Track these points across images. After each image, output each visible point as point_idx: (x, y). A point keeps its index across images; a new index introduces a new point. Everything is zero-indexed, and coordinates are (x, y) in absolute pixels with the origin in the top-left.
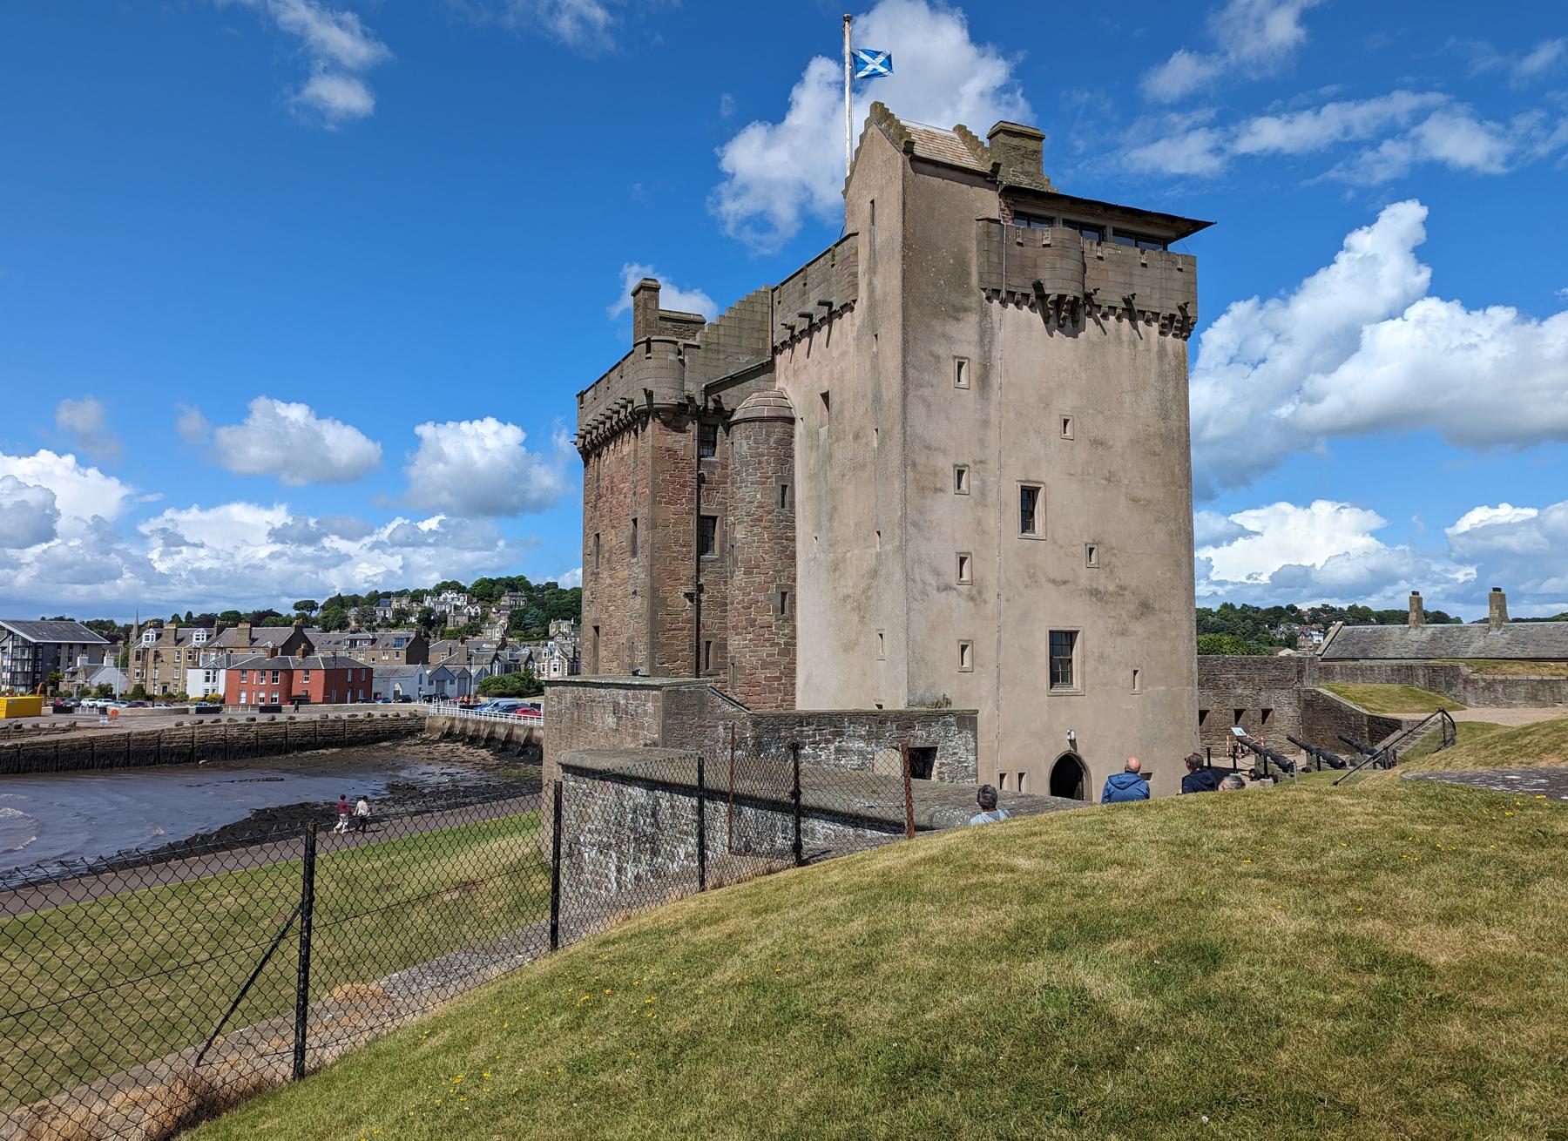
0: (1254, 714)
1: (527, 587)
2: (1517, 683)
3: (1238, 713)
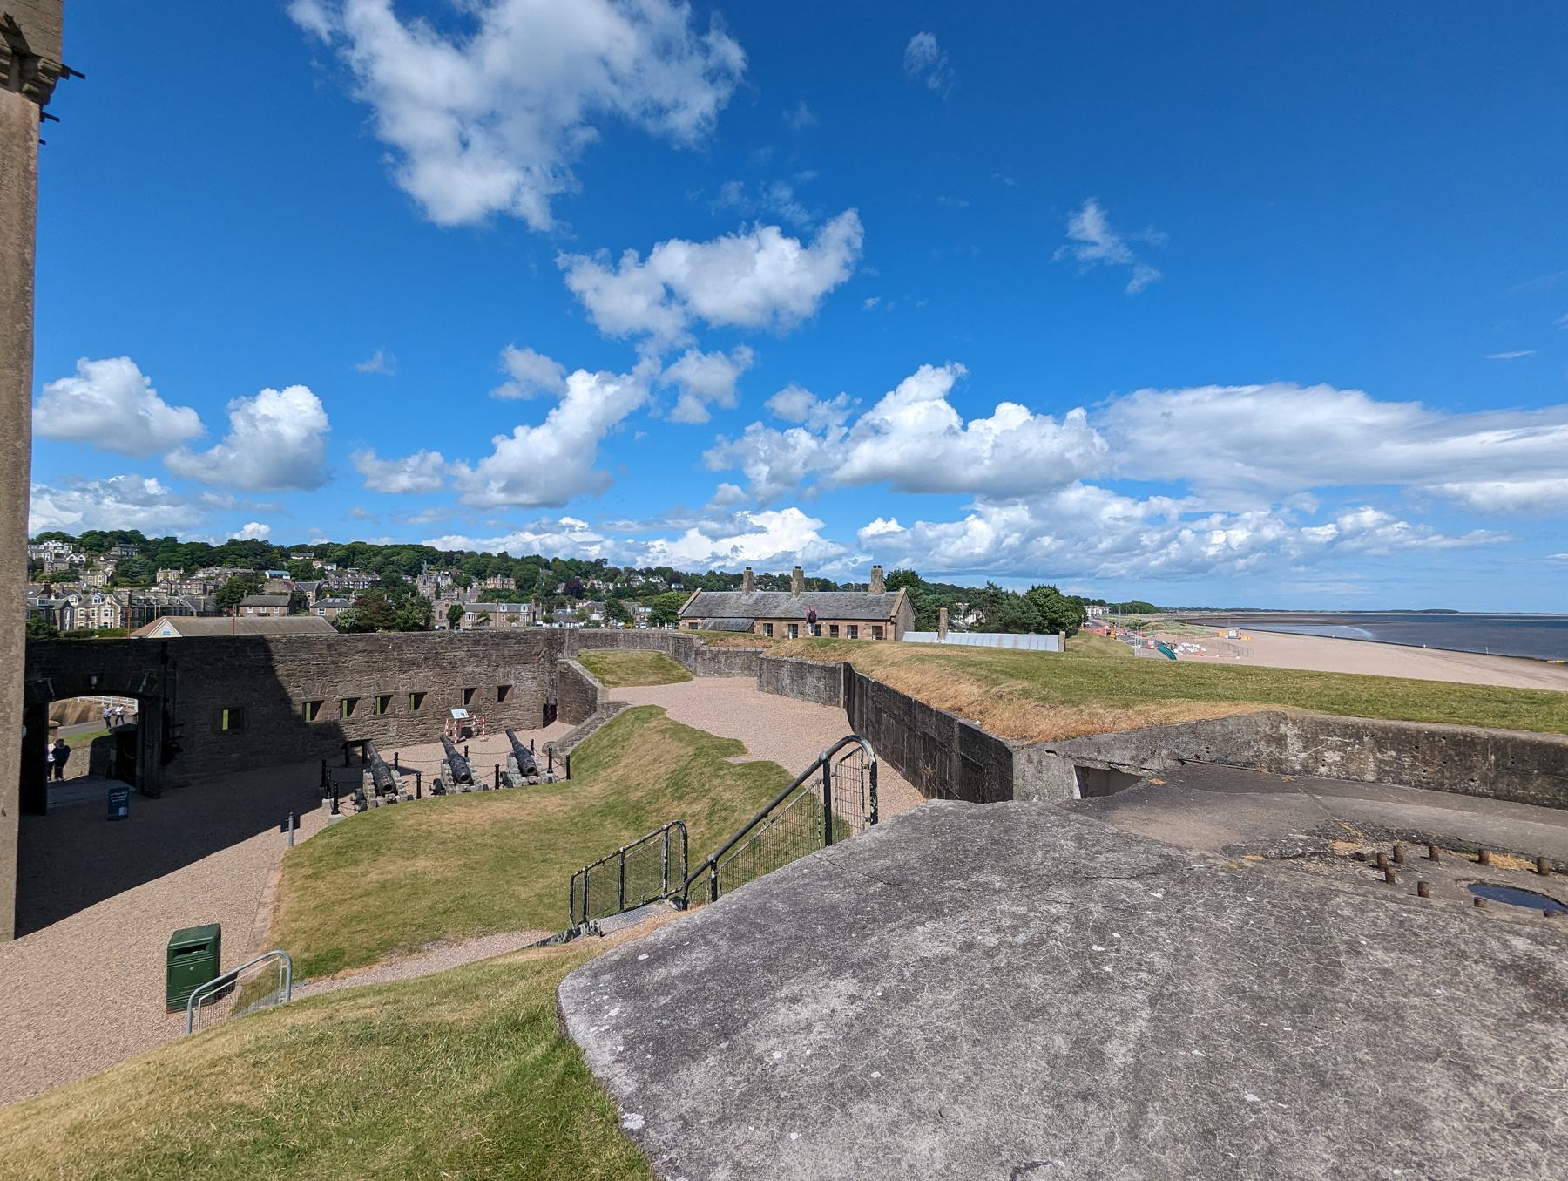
0: (486, 689)
1: (142, 540)
2: (736, 654)
3: (469, 693)
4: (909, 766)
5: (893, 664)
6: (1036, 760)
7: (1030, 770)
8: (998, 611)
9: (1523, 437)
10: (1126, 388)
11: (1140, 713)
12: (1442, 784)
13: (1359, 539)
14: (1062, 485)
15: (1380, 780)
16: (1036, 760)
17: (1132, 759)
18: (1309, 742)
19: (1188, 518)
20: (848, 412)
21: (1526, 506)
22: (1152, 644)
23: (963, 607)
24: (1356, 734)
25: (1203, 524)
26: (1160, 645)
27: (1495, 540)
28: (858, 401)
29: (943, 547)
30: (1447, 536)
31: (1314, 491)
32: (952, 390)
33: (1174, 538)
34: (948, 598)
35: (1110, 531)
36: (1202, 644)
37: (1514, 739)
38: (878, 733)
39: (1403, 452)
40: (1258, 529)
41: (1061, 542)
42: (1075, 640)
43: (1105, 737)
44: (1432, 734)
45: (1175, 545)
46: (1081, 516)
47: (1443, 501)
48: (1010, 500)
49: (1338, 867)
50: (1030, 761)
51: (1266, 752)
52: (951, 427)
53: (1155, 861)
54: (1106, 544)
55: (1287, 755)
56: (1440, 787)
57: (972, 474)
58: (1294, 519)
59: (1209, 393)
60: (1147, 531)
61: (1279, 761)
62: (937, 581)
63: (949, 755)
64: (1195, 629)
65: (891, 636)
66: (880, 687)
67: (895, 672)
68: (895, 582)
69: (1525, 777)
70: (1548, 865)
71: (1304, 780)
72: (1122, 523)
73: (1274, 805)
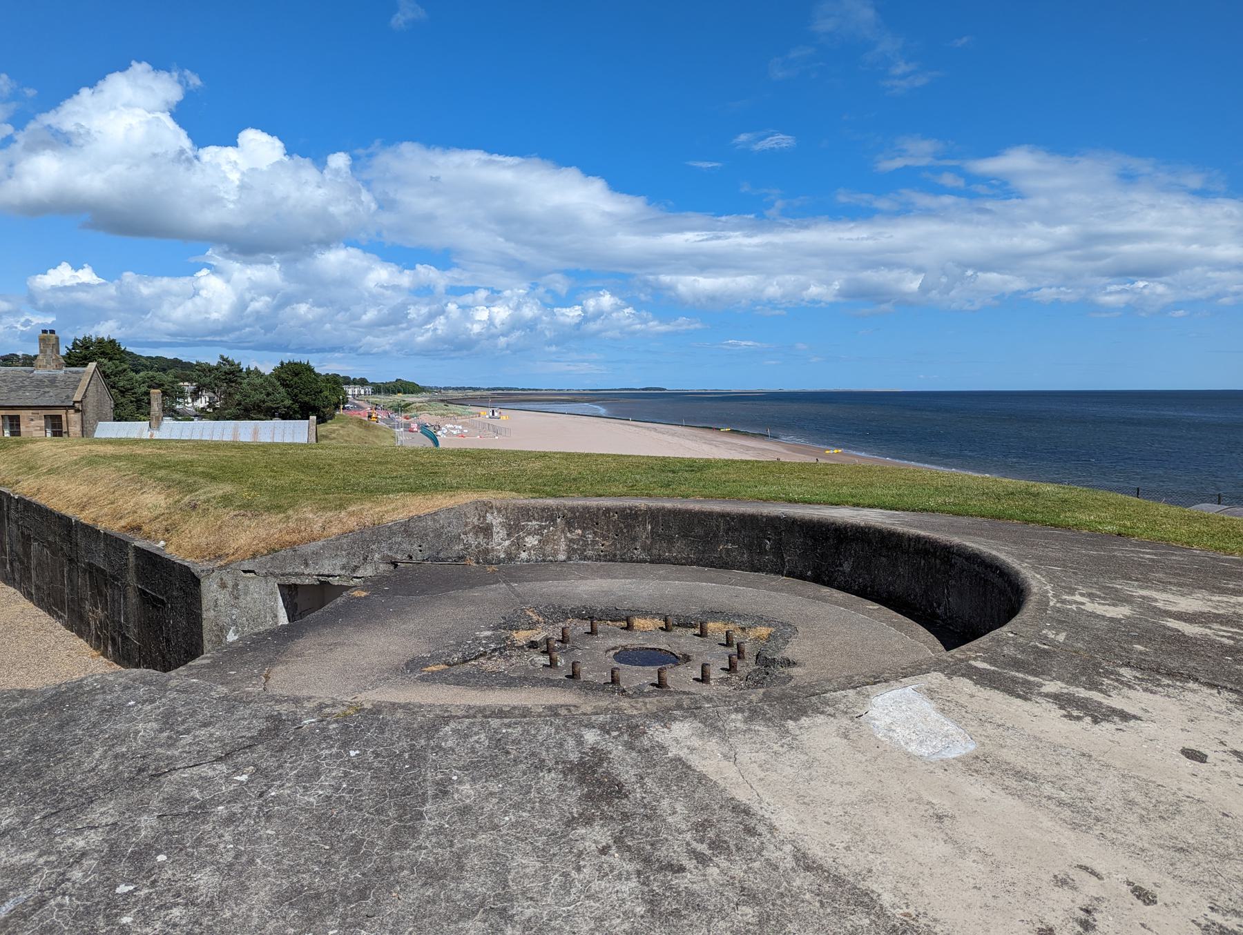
4: (72, 611)
5: (50, 471)
6: (230, 584)
7: (223, 597)
8: (234, 393)
9: (712, 239)
10: (392, 138)
11: (352, 514)
12: (615, 555)
13: (599, 321)
14: (326, 243)
15: (569, 558)
16: (230, 584)
17: (343, 568)
18: (513, 528)
19: (455, 291)
20: (13, 106)
21: (713, 298)
22: (414, 426)
23: (188, 387)
24: (549, 515)
25: (468, 299)
26: (424, 428)
27: (692, 327)
28: (31, 92)
29: (166, 308)
30: (661, 322)
31: (567, 273)
32: (179, 105)
33: (442, 312)
34: (167, 378)
35: (375, 300)
36: (464, 424)
37: (664, 508)
38: (28, 569)
39: (631, 243)
40: (518, 307)
41: (319, 311)
42: (323, 429)
43: (313, 546)
44: (608, 510)
45: (442, 319)
46: (343, 282)
47: (659, 291)
48: (261, 256)
49: (513, 660)
50: (223, 586)
51: (474, 543)
52: (182, 152)
53: (260, 724)
54: (370, 315)
55: (493, 544)
56: (613, 559)
57: (209, 218)
58: (548, 300)
59: (473, 158)
60: (415, 304)
61: (487, 551)
62: (154, 353)
63: (123, 590)
64: (458, 409)
65: (75, 429)
66: (27, 506)
67: (51, 482)
68: (83, 353)
69: (670, 540)
70: (672, 620)
71: (508, 569)
72: (388, 293)
73: (472, 602)
